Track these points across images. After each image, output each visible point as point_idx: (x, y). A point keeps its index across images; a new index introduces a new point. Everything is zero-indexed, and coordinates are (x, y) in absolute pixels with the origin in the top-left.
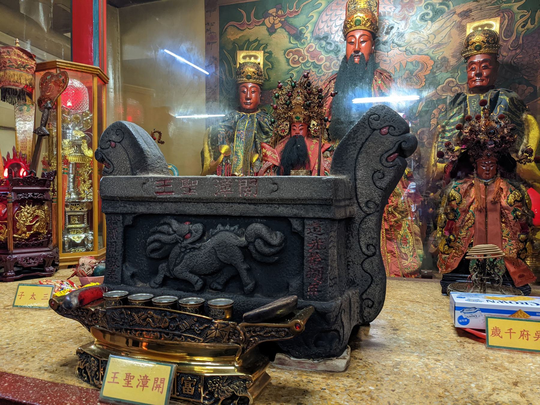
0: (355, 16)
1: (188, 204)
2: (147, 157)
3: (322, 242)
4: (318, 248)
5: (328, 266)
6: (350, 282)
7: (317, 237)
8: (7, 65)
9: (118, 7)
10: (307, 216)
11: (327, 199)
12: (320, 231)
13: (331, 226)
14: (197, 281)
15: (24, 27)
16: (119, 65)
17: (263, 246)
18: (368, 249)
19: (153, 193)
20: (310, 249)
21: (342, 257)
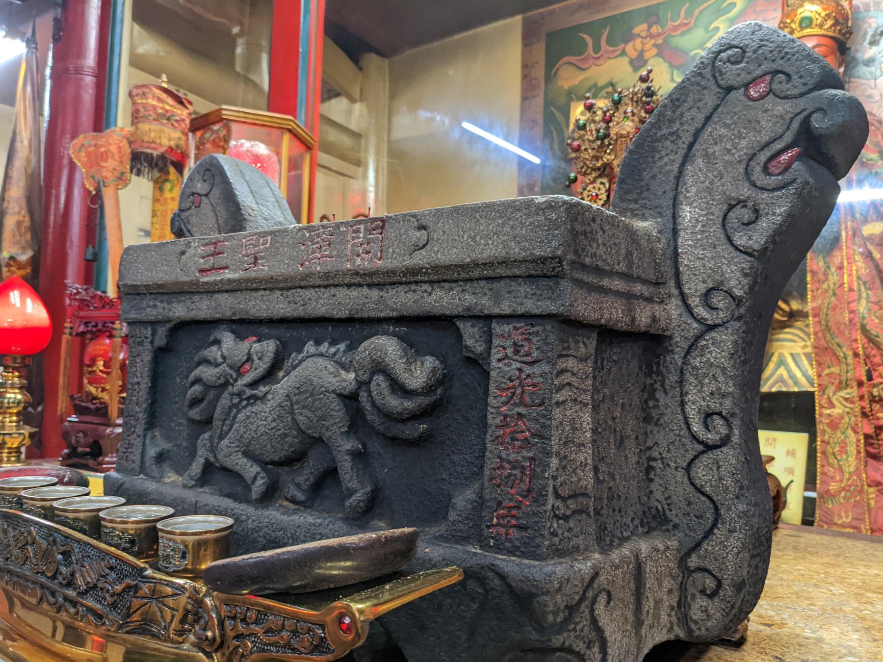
0: (799, 11)
1: (254, 294)
2: (245, 220)
3: (534, 385)
4: (522, 403)
5: (548, 454)
6: (654, 517)
7: (520, 370)
8: (141, 115)
9: (387, 57)
10: (497, 311)
11: (546, 259)
12: (528, 354)
13: (562, 341)
14: (255, 478)
15: (240, 90)
16: (385, 146)
17: (386, 392)
18: (707, 427)
19: (194, 273)
20: (505, 403)
21: (630, 443)
